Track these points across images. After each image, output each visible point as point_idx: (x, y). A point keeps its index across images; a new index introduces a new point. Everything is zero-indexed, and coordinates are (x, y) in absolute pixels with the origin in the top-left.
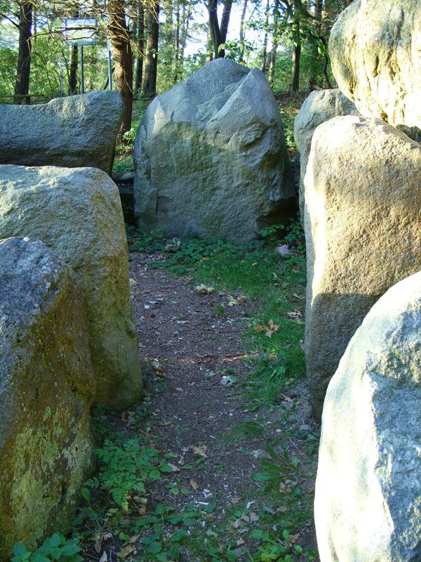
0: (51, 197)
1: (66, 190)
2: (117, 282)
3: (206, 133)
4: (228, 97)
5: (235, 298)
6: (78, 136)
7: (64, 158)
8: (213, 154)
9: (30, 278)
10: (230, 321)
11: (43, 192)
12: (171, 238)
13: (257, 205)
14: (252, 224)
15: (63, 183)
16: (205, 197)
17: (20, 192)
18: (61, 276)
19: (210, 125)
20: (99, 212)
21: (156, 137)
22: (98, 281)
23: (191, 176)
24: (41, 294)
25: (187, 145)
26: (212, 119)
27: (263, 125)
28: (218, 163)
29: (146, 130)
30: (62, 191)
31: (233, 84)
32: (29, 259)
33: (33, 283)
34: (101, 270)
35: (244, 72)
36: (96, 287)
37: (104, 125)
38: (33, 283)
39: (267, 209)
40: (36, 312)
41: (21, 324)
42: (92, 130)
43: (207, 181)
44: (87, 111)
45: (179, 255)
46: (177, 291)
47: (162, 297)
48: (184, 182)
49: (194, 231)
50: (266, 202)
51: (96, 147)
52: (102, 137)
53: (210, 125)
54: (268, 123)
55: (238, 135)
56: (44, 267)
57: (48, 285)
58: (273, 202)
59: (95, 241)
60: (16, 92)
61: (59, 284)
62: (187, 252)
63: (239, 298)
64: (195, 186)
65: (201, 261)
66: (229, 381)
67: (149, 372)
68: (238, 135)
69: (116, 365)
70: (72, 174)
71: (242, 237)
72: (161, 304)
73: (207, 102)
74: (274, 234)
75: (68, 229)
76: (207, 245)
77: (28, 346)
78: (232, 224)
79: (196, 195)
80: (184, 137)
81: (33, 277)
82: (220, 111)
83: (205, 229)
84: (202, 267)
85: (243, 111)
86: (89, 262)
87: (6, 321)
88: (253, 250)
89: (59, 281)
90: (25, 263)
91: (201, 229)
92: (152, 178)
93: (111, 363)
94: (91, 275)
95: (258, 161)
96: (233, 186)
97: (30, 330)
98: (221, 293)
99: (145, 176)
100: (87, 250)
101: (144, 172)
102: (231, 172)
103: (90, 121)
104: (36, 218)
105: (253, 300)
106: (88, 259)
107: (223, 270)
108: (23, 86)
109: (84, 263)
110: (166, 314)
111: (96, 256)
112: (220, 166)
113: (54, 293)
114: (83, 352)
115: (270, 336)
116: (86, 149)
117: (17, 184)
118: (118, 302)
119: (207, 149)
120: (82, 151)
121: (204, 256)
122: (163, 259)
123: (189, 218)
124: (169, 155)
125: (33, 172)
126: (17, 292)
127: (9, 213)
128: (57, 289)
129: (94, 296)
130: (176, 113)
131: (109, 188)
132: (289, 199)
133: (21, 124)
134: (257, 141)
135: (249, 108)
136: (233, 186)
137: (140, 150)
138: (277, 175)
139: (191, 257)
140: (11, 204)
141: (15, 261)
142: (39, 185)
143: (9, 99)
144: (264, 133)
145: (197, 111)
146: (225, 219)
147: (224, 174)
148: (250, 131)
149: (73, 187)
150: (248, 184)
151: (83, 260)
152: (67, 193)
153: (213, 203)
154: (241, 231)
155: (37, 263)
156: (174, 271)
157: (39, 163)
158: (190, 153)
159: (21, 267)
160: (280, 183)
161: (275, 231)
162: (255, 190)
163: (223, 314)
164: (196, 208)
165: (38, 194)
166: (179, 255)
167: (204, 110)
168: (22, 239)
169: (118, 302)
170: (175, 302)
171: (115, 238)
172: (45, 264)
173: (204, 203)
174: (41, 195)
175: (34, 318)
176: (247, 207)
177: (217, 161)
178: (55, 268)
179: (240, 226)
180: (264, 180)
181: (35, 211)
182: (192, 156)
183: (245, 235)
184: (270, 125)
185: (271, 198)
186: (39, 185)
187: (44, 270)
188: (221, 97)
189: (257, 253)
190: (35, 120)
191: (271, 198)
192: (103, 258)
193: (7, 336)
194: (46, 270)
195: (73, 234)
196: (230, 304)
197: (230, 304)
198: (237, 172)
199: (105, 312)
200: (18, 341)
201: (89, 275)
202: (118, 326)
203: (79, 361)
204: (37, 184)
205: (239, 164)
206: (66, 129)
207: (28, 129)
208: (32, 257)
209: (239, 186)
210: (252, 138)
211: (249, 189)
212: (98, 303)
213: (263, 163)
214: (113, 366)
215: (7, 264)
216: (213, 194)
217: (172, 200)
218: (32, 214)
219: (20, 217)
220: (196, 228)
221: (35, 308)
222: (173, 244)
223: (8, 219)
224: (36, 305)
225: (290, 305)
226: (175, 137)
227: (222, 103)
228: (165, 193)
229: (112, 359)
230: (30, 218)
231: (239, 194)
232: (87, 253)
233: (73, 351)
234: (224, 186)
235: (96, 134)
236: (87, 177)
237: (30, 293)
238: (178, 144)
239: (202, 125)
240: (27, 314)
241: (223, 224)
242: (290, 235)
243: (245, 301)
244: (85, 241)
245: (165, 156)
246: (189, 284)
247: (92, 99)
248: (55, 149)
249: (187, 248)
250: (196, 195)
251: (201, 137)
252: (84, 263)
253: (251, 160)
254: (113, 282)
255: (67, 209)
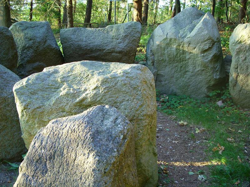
0: (118, 81)
1: (127, 77)
2: (151, 128)
3: (184, 44)
4: (195, 26)
5: (199, 129)
6: (120, 43)
7: (112, 54)
8: (187, 54)
9: (111, 133)
10: (198, 142)
11: (114, 77)
12: (162, 94)
13: (207, 81)
14: (204, 90)
15: (125, 73)
16: (181, 76)
17: (101, 78)
18: (128, 130)
19: (186, 40)
20: (144, 90)
21: (158, 45)
22: (142, 128)
23: (175, 65)
24: (118, 143)
25: (174, 49)
26: (187, 37)
27: (213, 41)
28: (188, 59)
29: (153, 41)
30: (124, 78)
31: (197, 20)
32: (110, 120)
33: (114, 135)
34: (144, 122)
35: (202, 14)
36: (140, 131)
37: (133, 39)
38: (114, 135)
39: (212, 83)
40: (115, 154)
41: (107, 162)
42: (127, 41)
43: (183, 67)
44: (125, 32)
45: (168, 104)
46: (168, 124)
47: (161, 126)
48: (171, 68)
49: (174, 92)
50: (212, 79)
51: (128, 49)
52: (131, 44)
53: (186, 40)
54: (215, 40)
55: (200, 45)
56: (119, 126)
57: (122, 136)
58: (216, 79)
59: (142, 106)
60: (85, 22)
61: (127, 135)
62: (172, 103)
63: (201, 129)
64: (176, 70)
65: (179, 107)
66: (203, 178)
67: (160, 171)
68: (200, 45)
69: (146, 171)
70: (130, 68)
71: (199, 96)
72: (161, 130)
73: (184, 29)
74: (215, 95)
75: (127, 99)
76: (181, 99)
77: (110, 175)
78: (194, 89)
79: (177, 74)
80: (172, 46)
81: (113, 132)
82: (191, 33)
83: (180, 91)
84: (179, 111)
85: (203, 33)
86: (137, 118)
87: (98, 161)
88: (204, 103)
89: (127, 133)
90: (108, 123)
91: (178, 91)
92: (155, 65)
93: (144, 170)
94: (138, 124)
95: (210, 59)
96: (196, 70)
97: (112, 166)
98: (191, 126)
99: (151, 64)
100: (137, 110)
101: (151, 62)
102: (195, 64)
103: (126, 36)
104: (110, 92)
105: (208, 131)
106: (137, 116)
107: (191, 113)
108: (88, 19)
109: (135, 118)
110: (164, 136)
111: (141, 114)
112: (190, 61)
113: (124, 142)
114: (134, 170)
115: (221, 154)
116: (124, 50)
117: (100, 72)
118: (151, 138)
119: (184, 52)
120: (121, 51)
121: (180, 105)
122: (159, 106)
123: (172, 85)
124: (164, 54)
125: (107, 65)
126: (104, 142)
127: (95, 89)
128: (126, 139)
129: (139, 136)
130: (168, 34)
131: (149, 76)
132: (223, 77)
133: (92, 37)
134: (210, 49)
135: (206, 32)
136: (196, 70)
137: (150, 51)
138: (218, 65)
139: (174, 105)
140: (96, 84)
141: (102, 121)
142: (112, 74)
143: (81, 25)
144: (213, 44)
145: (179, 33)
146: (190, 87)
147: (191, 65)
148: (206, 44)
149: (131, 75)
150: (203, 70)
151: (134, 116)
152: (127, 79)
153: (185, 79)
154: (198, 93)
155: (115, 122)
156: (166, 113)
157: (105, 60)
158: (175, 54)
159: (106, 125)
160: (219, 70)
161: (216, 93)
162: (207, 73)
163: (194, 138)
164: (176, 81)
165: (111, 79)
166: (168, 104)
167: (183, 33)
168: (104, 106)
169: (151, 138)
170: (168, 130)
171: (151, 106)
172: (119, 124)
173: (180, 78)
174: (113, 79)
175: (114, 158)
176: (202, 81)
177: (188, 58)
178: (125, 126)
179: (198, 90)
180: (212, 68)
181: (109, 88)
182: (176, 55)
183: (200, 95)
184: (216, 41)
185: (215, 77)
186: (112, 74)
187: (119, 127)
188: (191, 26)
189: (207, 105)
190: (99, 36)
191: (215, 77)
192: (145, 115)
193: (98, 170)
194: (120, 127)
195: (130, 102)
196: (197, 132)
197: (197, 132)
198: (198, 63)
199: (143, 144)
200: (105, 173)
201: (137, 124)
202: (149, 150)
203: (133, 176)
204: (111, 73)
205: (200, 60)
206: (114, 40)
207: (95, 40)
208: (111, 119)
209: (199, 71)
210: (207, 47)
211: (204, 72)
212: (141, 139)
213: (212, 59)
214: (145, 172)
215: (98, 123)
216: (185, 74)
217: (164, 76)
218: (107, 90)
219: (101, 91)
220: (175, 90)
221: (115, 152)
222: (164, 98)
223: (95, 92)
224: (115, 150)
225: (228, 134)
226: (168, 45)
227: (191, 29)
228: (161, 72)
229: (146, 168)
230: (106, 92)
231: (198, 74)
232: (137, 112)
233: (130, 170)
234: (191, 70)
235: (128, 43)
236: (138, 70)
237: (112, 142)
238: (169, 49)
239: (182, 39)
240: (110, 156)
241: (189, 89)
242: (224, 96)
243: (204, 131)
244: (136, 106)
245: (162, 55)
246: (174, 120)
247: (127, 26)
248: (108, 50)
249: (171, 101)
250: (177, 74)
251: (181, 46)
252: (135, 118)
253: (206, 58)
254: (149, 128)
255: (127, 88)
